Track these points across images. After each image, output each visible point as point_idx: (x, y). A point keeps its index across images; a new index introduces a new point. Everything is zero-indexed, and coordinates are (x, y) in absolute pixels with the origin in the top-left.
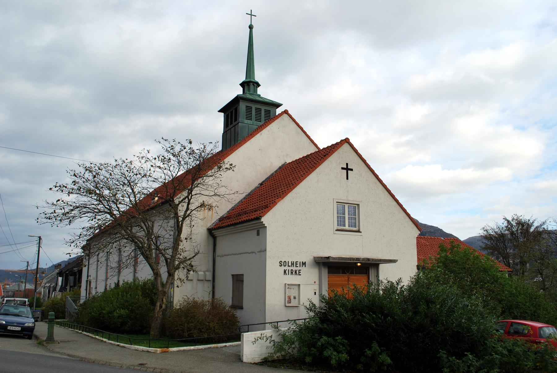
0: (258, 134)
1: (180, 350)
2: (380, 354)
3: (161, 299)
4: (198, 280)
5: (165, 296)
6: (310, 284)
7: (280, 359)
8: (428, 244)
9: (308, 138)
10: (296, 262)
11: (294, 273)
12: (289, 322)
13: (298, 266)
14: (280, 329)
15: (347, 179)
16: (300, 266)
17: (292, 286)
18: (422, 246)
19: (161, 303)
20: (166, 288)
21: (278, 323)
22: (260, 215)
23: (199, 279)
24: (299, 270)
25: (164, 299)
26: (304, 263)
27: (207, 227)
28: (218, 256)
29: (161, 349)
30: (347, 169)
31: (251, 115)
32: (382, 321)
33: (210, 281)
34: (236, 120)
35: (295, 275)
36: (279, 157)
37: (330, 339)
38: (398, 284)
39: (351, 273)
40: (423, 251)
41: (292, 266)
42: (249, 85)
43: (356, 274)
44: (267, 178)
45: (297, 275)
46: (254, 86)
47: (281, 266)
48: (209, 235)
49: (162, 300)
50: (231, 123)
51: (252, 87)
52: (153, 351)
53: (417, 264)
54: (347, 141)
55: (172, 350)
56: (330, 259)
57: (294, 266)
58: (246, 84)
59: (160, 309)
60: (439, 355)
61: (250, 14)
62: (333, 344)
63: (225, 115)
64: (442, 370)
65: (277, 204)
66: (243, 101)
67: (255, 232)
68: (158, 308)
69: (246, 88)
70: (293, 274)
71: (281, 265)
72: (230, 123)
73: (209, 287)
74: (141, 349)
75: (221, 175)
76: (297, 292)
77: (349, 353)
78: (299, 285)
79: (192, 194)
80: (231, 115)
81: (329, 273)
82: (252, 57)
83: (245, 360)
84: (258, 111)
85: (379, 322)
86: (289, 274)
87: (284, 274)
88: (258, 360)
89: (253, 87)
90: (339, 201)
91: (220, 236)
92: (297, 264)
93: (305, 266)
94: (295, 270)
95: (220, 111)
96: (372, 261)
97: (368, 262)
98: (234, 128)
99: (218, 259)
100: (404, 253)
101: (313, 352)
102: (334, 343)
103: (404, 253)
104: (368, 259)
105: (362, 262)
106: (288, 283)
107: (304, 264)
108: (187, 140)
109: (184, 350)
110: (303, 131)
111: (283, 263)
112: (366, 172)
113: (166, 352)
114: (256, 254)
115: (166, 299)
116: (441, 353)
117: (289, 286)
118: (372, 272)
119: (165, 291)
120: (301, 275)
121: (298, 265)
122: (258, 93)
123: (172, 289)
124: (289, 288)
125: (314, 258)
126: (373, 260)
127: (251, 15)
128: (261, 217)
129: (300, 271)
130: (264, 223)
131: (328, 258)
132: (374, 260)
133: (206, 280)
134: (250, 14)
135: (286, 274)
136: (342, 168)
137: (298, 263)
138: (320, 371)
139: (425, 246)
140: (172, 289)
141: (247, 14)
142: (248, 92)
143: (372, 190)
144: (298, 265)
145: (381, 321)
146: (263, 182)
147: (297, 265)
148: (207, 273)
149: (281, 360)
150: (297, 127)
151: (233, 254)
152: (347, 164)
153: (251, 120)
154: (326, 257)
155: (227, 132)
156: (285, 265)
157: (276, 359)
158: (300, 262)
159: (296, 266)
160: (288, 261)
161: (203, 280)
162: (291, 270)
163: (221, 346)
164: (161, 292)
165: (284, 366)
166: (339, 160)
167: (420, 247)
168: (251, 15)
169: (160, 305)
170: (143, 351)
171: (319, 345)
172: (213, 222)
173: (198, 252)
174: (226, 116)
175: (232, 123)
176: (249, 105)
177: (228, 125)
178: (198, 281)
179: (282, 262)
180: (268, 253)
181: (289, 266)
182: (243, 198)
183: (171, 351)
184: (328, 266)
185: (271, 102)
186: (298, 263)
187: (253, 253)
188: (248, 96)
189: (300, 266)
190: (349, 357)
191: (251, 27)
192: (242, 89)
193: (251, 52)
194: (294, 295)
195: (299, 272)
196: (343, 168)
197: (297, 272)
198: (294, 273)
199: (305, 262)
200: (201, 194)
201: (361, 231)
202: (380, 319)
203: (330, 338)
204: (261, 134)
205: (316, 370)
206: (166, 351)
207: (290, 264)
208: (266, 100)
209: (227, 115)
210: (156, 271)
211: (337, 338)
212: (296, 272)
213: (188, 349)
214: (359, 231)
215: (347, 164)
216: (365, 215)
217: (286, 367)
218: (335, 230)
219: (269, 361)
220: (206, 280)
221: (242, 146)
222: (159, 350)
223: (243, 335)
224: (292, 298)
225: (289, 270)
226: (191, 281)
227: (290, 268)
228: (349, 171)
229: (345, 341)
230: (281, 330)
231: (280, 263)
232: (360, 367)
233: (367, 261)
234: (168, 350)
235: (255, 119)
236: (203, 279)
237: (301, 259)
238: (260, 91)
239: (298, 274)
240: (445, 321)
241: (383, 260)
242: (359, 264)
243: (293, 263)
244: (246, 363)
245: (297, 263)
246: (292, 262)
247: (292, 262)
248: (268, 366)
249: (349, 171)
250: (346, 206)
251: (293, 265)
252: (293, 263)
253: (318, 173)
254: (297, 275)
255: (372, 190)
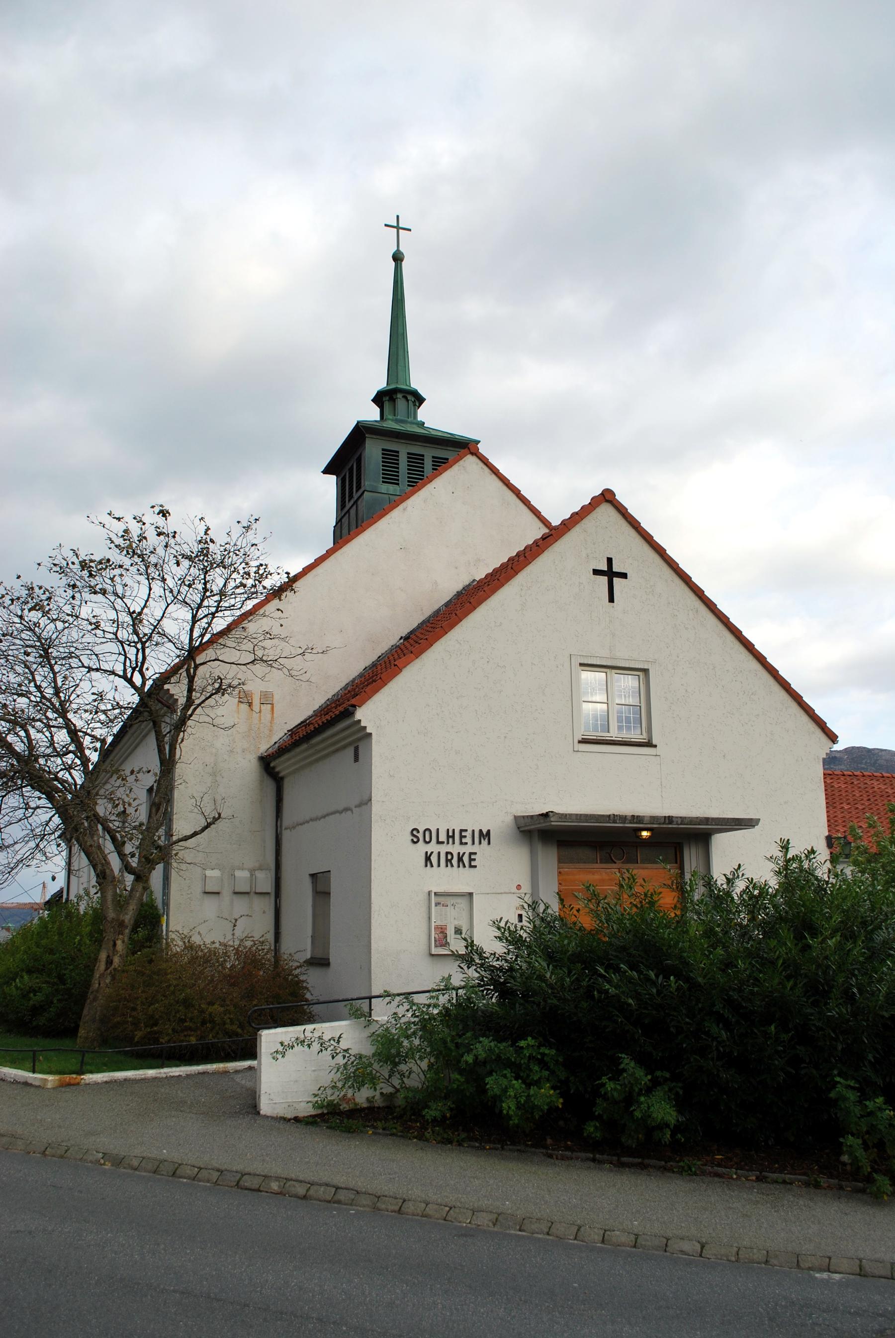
0: (397, 509)
1: (116, 1081)
2: (649, 1090)
3: (112, 943)
4: (206, 893)
5: (122, 934)
6: (505, 893)
7: (374, 1107)
8: (891, 791)
9: (534, 516)
10: (461, 831)
11: (455, 861)
12: (388, 999)
13: (466, 843)
14: (375, 1019)
15: (611, 599)
16: (473, 843)
17: (451, 897)
18: (875, 796)
19: (111, 954)
20: (126, 914)
21: (373, 1000)
22: (353, 701)
23: (237, 890)
24: (471, 854)
25: (119, 943)
26: (485, 833)
27: (259, 754)
28: (286, 829)
29: (57, 1077)
30: (610, 574)
31: (398, 472)
32: (658, 991)
33: (267, 897)
34: (360, 488)
35: (459, 866)
36: (456, 568)
37: (502, 1046)
38: (729, 881)
39: (629, 861)
40: (875, 809)
41: (448, 843)
42: (393, 400)
43: (643, 862)
44: (423, 622)
45: (464, 866)
46: (408, 401)
47: (415, 843)
48: (265, 775)
49: (115, 945)
50: (351, 497)
51: (401, 403)
52: (37, 1083)
53: (827, 834)
54: (607, 497)
55: (89, 1079)
56: (552, 819)
57: (454, 843)
58: (387, 398)
59: (107, 969)
60: (832, 1095)
61: (396, 225)
62: (513, 1060)
63: (340, 479)
64: (841, 1140)
65: (400, 670)
66: (374, 437)
67: (350, 751)
68: (102, 966)
69: (387, 405)
70: (452, 866)
71: (415, 840)
72: (349, 496)
73: (264, 912)
74: (12, 1076)
75: (282, 612)
76: (465, 915)
77: (561, 1087)
78: (471, 895)
79: (195, 663)
80: (349, 477)
81: (560, 861)
82: (400, 331)
83: (265, 1108)
84: (416, 460)
85: (650, 994)
86: (439, 866)
87: (426, 866)
88: (305, 1110)
89: (406, 403)
90: (586, 662)
91: (290, 774)
92: (465, 837)
93: (489, 843)
94: (459, 853)
95: (327, 471)
96: (681, 824)
97: (670, 826)
98: (355, 507)
99: (286, 835)
100: (786, 803)
101: (455, 1086)
102: (515, 1059)
103: (786, 803)
104: (670, 819)
105: (649, 826)
106: (435, 890)
107: (485, 836)
108: (153, 507)
109: (125, 1080)
110: (520, 499)
111: (420, 835)
112: (666, 581)
113: (74, 1085)
114: (352, 811)
115: (123, 942)
116: (839, 1088)
117: (441, 900)
118: (691, 860)
119: (123, 921)
120: (475, 867)
121: (468, 840)
122: (419, 419)
123: (165, 916)
124: (439, 904)
125: (516, 818)
126: (683, 820)
127: (398, 228)
128: (354, 706)
129: (473, 857)
130: (363, 724)
131: (546, 815)
132: (686, 821)
133: (256, 893)
134: (396, 225)
135: (432, 866)
136: (594, 570)
137: (468, 834)
138: (477, 1145)
139: (882, 796)
140: (165, 916)
141: (386, 225)
142: (390, 417)
143: (687, 629)
144: (468, 840)
145: (654, 991)
146: (411, 632)
147: (464, 840)
148: (260, 875)
149: (379, 1108)
150: (505, 488)
151: (312, 820)
152: (610, 561)
153: (398, 484)
154: (542, 815)
155: (343, 520)
156: (427, 839)
157: (365, 1105)
158: (473, 831)
159: (461, 843)
160: (438, 829)
161: (248, 893)
162: (447, 853)
163: (239, 1068)
164: (112, 922)
165: (375, 1128)
166: (586, 548)
167: (869, 800)
168: (398, 228)
169: (108, 957)
170: (16, 1082)
171: (466, 1062)
172: (275, 738)
173: (217, 816)
174: (340, 483)
175: (352, 497)
176: (392, 446)
177: (345, 502)
178: (235, 897)
179: (418, 832)
180: (376, 808)
181: (438, 842)
182: (357, 674)
183: (87, 1082)
184: (558, 841)
185: (449, 436)
186: (468, 834)
187: (347, 809)
188: (390, 425)
189: (473, 843)
190: (561, 1100)
191: (398, 258)
192: (378, 410)
193: (397, 320)
194: (456, 923)
195: (471, 860)
196: (596, 572)
197: (466, 859)
198: (455, 861)
199: (489, 831)
200: (218, 660)
201: (654, 743)
202: (654, 983)
203: (504, 1044)
204: (404, 509)
205: (463, 1140)
206: (72, 1082)
207: (443, 838)
208: (433, 433)
209: (342, 479)
210: (99, 867)
211: (522, 1043)
212: (460, 859)
213: (138, 1077)
214: (649, 744)
215: (610, 561)
216: (666, 699)
217: (381, 1131)
218: (576, 741)
219: (341, 1114)
220: (256, 893)
221: (354, 541)
222: (51, 1079)
223: (261, 1036)
224: (450, 932)
225: (439, 853)
226: (217, 895)
227: (444, 849)
228: (616, 580)
229: (547, 1051)
230: (377, 1021)
231: (413, 835)
232: (592, 1129)
233: (663, 824)
234: (77, 1081)
235: (409, 481)
236: (248, 890)
237: (475, 824)
238: (424, 414)
239: (467, 864)
240: (859, 989)
241: (713, 819)
242: (645, 834)
243: (451, 834)
244: (268, 1117)
245: (463, 834)
246: (448, 830)
247: (448, 830)
248: (327, 1127)
249: (616, 580)
250: (608, 674)
251: (451, 840)
252: (451, 834)
253: (522, 586)
254: (464, 866)
255: (687, 629)
